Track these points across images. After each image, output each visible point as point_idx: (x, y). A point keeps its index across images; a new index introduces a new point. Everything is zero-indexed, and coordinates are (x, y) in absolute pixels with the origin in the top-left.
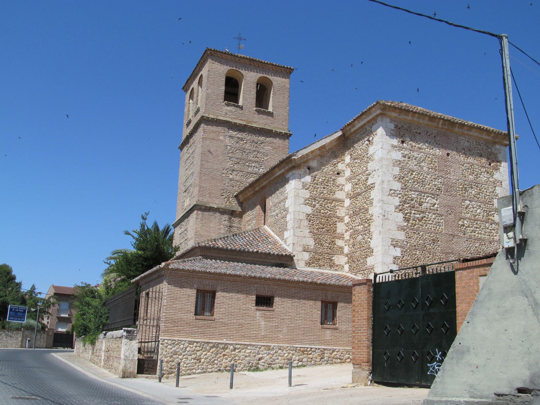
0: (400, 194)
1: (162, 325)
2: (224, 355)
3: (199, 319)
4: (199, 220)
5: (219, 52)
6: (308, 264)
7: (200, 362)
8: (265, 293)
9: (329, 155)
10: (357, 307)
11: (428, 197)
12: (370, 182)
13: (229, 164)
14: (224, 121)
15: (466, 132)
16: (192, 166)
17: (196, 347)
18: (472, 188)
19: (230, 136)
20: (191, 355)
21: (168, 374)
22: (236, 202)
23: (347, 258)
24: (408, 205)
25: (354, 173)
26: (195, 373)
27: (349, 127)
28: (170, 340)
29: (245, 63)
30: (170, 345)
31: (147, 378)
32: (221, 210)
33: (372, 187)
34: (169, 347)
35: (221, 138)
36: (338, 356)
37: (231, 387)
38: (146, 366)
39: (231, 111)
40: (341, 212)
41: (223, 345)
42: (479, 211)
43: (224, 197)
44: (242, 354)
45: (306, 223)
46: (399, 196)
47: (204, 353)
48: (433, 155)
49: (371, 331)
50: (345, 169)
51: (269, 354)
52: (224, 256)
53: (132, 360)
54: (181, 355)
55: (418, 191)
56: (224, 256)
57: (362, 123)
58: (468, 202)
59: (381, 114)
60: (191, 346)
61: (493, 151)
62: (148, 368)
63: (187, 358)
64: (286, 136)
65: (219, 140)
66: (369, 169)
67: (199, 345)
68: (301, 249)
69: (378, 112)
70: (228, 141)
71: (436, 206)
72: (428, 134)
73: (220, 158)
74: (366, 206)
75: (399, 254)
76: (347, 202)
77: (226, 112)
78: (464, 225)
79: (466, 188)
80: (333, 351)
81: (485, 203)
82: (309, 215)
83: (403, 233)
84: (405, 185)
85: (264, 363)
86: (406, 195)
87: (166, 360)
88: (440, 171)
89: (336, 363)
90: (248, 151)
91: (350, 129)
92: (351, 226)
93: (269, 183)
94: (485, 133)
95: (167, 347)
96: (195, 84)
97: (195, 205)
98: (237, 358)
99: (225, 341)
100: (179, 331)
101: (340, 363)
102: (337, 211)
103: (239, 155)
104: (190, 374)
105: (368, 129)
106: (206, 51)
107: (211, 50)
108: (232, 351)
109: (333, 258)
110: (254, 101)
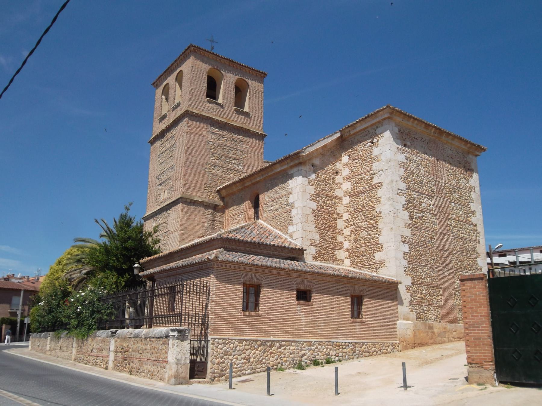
0: (406, 193)
1: (211, 323)
2: (271, 353)
3: (246, 316)
4: (184, 213)
5: (202, 49)
6: (315, 258)
7: (249, 361)
8: (304, 287)
9: (328, 154)
10: (469, 303)
11: (425, 197)
12: (375, 181)
13: (211, 160)
14: (207, 117)
15: (450, 141)
16: (170, 159)
17: (245, 345)
18: (455, 192)
19: (212, 133)
20: (241, 355)
21: (219, 377)
22: (218, 197)
23: (347, 253)
24: (411, 205)
25: (354, 173)
26: (245, 375)
27: (350, 129)
28: (220, 339)
29: (225, 63)
30: (221, 344)
31: (199, 382)
32: (205, 204)
33: (379, 185)
34: (220, 346)
35: (204, 133)
36: (366, 349)
37: (337, 393)
38: (197, 370)
39: (212, 108)
40: (340, 209)
41: (270, 343)
42: (461, 213)
43: (207, 191)
44: (287, 351)
45: (312, 218)
46: (405, 195)
47: (253, 352)
48: (427, 160)
49: (490, 329)
50: (342, 168)
51: (311, 350)
52: (243, 248)
53: (184, 364)
54: (231, 355)
55: (418, 192)
56: (243, 248)
57: (364, 126)
58: (453, 204)
59: (388, 118)
60: (241, 345)
61: (468, 160)
62: (198, 371)
63: (237, 359)
64: (261, 137)
65: (202, 135)
66: (374, 168)
67: (248, 343)
68: (309, 243)
69: (386, 116)
70: (211, 138)
71: (431, 206)
72: (423, 140)
73: (203, 152)
74: (371, 204)
75: (407, 250)
76: (346, 200)
77: (207, 108)
78: (451, 225)
79: (451, 191)
80: (363, 345)
81: (465, 206)
82: (314, 210)
83: (409, 230)
84: (409, 186)
85: (307, 359)
86: (410, 195)
87: (217, 361)
88: (433, 175)
89: (365, 357)
90: (229, 148)
91: (349, 131)
92: (352, 223)
93: (264, 179)
94: (463, 143)
95: (217, 347)
96: (171, 80)
97: (181, 198)
98: (283, 356)
99: (271, 338)
100: (228, 329)
101: (369, 356)
102: (337, 207)
103: (220, 151)
104: (240, 376)
105: (371, 131)
106: (189, 47)
107: (195, 46)
108: (278, 349)
109: (335, 253)
110: (233, 101)
